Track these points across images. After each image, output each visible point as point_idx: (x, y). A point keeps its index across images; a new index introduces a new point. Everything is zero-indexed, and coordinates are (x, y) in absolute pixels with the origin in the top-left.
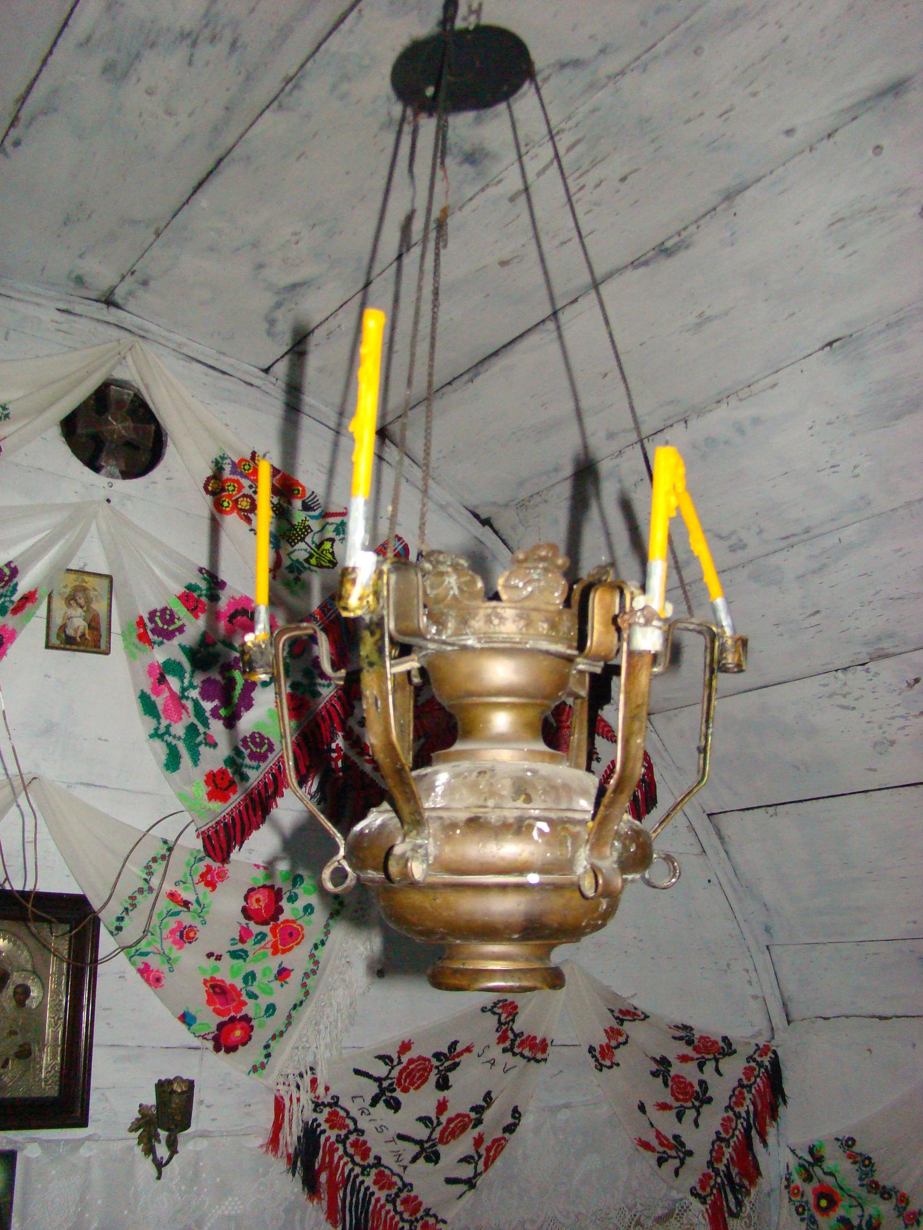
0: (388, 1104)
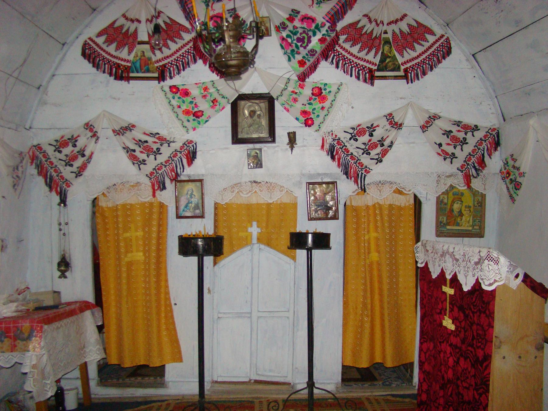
0: (354, 140)
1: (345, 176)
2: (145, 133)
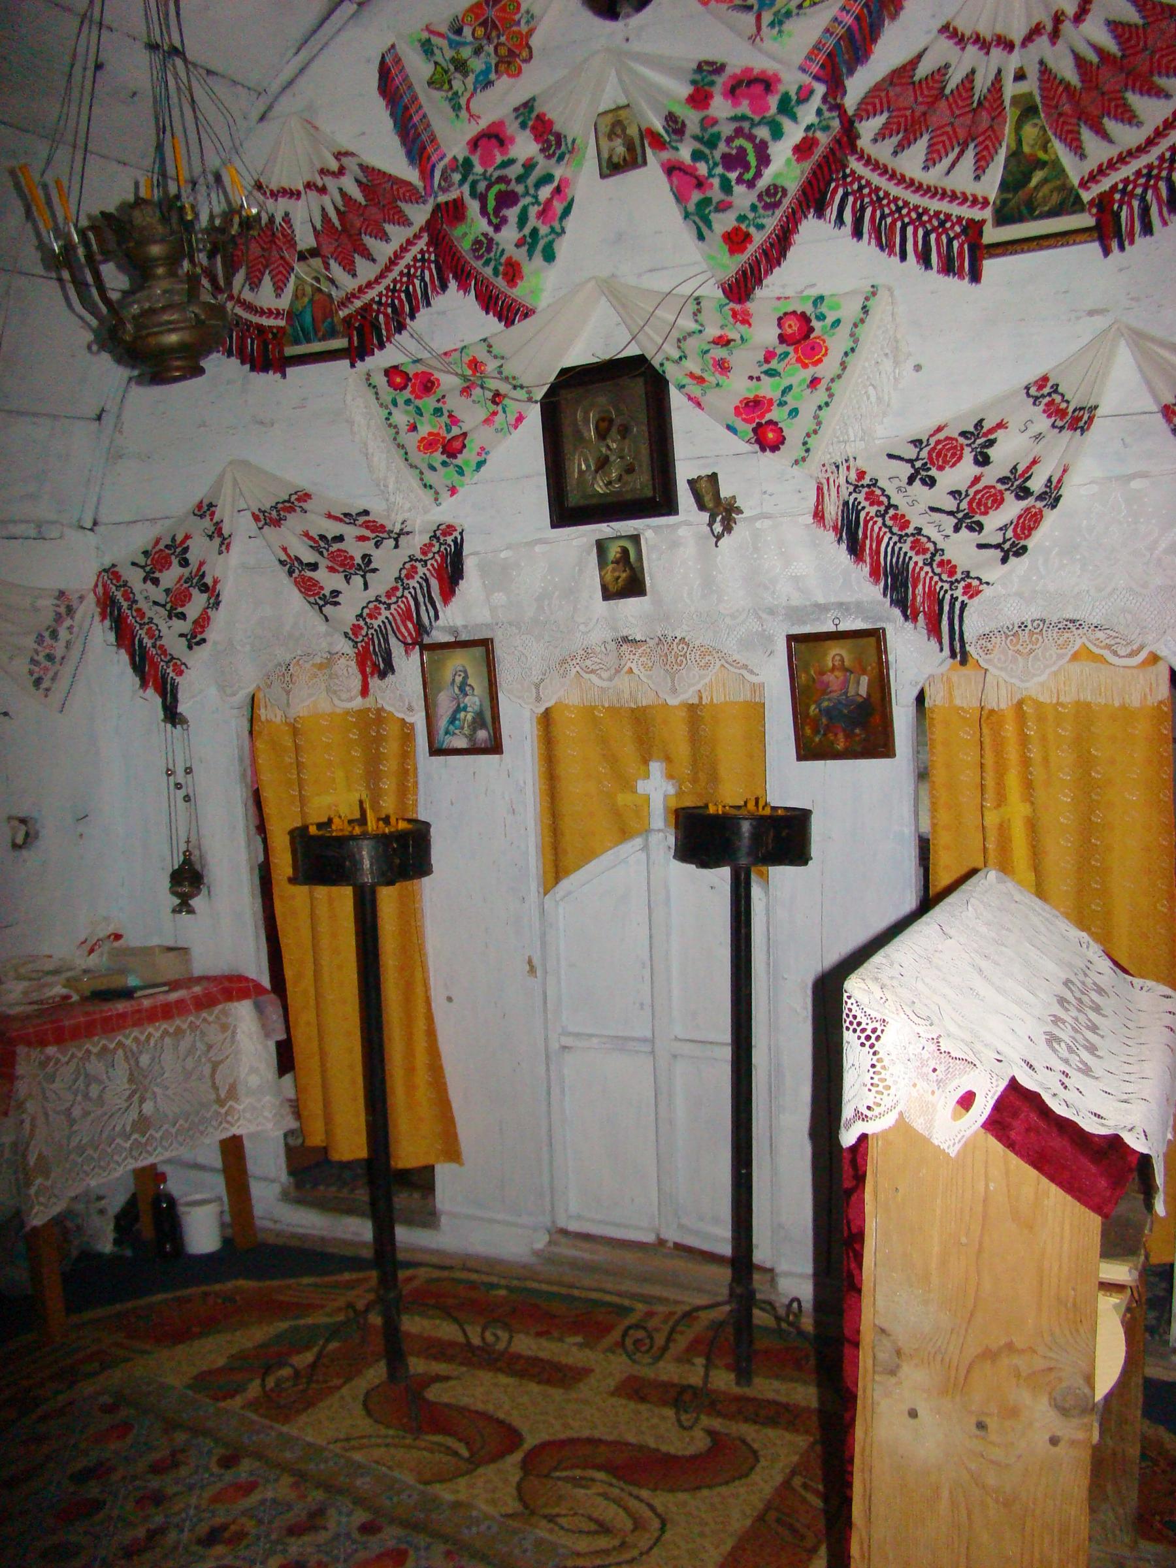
1: (897, 612)
2: (330, 516)
